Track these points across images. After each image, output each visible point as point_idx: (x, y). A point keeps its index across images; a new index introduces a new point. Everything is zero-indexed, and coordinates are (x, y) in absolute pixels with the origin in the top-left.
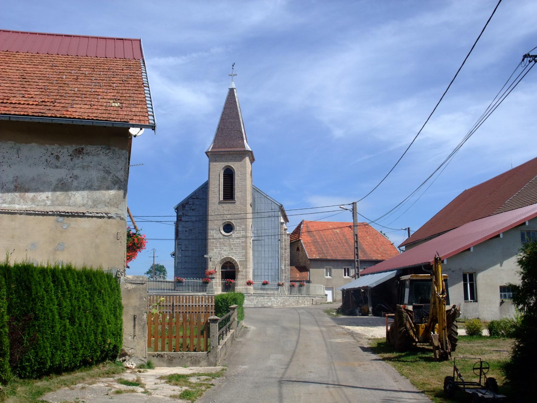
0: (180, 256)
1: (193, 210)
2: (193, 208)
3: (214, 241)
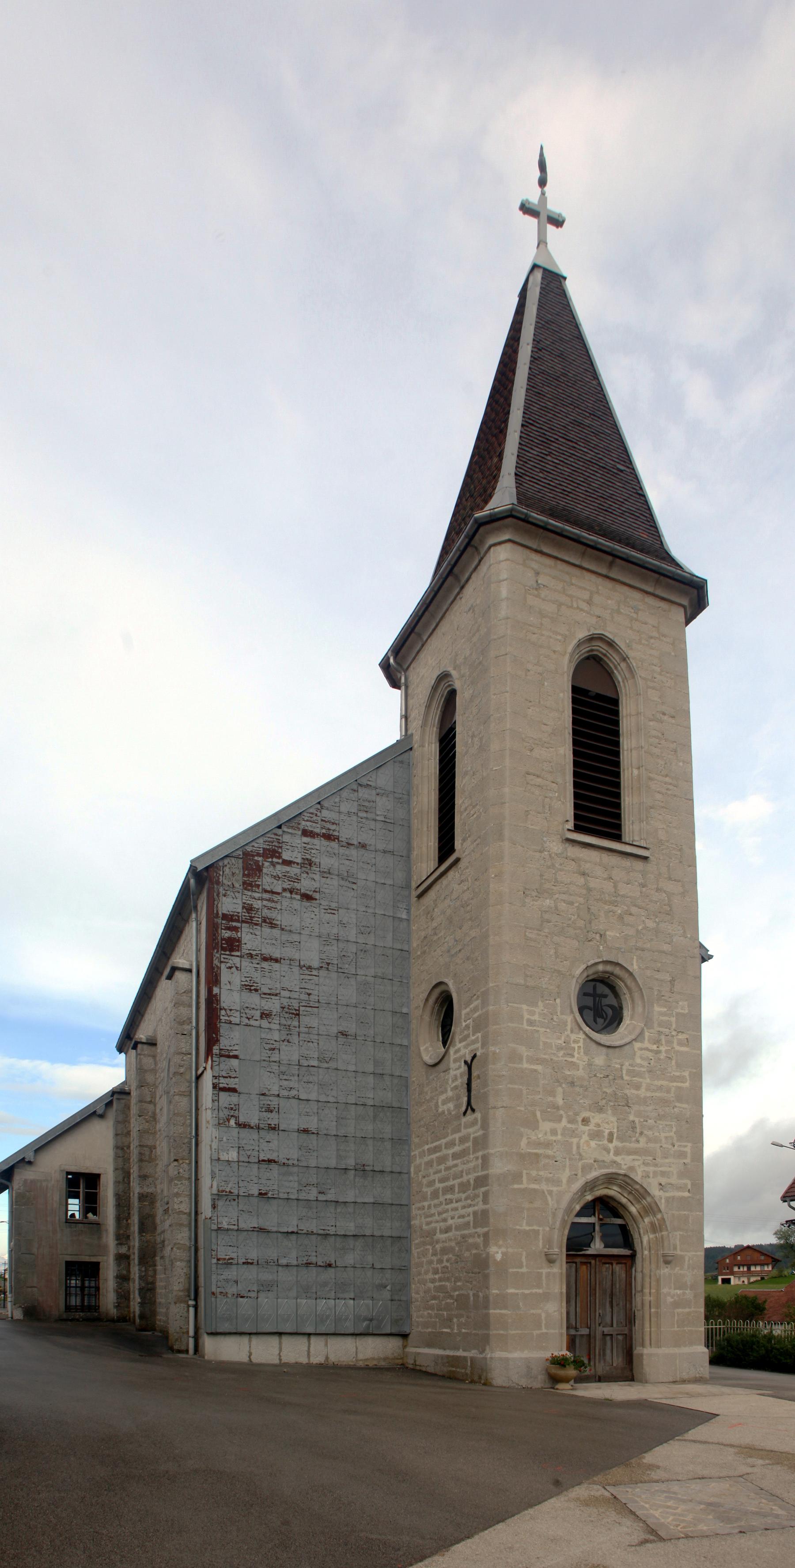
0: (233, 1155)
1: (307, 897)
2: (306, 884)
3: (539, 1068)
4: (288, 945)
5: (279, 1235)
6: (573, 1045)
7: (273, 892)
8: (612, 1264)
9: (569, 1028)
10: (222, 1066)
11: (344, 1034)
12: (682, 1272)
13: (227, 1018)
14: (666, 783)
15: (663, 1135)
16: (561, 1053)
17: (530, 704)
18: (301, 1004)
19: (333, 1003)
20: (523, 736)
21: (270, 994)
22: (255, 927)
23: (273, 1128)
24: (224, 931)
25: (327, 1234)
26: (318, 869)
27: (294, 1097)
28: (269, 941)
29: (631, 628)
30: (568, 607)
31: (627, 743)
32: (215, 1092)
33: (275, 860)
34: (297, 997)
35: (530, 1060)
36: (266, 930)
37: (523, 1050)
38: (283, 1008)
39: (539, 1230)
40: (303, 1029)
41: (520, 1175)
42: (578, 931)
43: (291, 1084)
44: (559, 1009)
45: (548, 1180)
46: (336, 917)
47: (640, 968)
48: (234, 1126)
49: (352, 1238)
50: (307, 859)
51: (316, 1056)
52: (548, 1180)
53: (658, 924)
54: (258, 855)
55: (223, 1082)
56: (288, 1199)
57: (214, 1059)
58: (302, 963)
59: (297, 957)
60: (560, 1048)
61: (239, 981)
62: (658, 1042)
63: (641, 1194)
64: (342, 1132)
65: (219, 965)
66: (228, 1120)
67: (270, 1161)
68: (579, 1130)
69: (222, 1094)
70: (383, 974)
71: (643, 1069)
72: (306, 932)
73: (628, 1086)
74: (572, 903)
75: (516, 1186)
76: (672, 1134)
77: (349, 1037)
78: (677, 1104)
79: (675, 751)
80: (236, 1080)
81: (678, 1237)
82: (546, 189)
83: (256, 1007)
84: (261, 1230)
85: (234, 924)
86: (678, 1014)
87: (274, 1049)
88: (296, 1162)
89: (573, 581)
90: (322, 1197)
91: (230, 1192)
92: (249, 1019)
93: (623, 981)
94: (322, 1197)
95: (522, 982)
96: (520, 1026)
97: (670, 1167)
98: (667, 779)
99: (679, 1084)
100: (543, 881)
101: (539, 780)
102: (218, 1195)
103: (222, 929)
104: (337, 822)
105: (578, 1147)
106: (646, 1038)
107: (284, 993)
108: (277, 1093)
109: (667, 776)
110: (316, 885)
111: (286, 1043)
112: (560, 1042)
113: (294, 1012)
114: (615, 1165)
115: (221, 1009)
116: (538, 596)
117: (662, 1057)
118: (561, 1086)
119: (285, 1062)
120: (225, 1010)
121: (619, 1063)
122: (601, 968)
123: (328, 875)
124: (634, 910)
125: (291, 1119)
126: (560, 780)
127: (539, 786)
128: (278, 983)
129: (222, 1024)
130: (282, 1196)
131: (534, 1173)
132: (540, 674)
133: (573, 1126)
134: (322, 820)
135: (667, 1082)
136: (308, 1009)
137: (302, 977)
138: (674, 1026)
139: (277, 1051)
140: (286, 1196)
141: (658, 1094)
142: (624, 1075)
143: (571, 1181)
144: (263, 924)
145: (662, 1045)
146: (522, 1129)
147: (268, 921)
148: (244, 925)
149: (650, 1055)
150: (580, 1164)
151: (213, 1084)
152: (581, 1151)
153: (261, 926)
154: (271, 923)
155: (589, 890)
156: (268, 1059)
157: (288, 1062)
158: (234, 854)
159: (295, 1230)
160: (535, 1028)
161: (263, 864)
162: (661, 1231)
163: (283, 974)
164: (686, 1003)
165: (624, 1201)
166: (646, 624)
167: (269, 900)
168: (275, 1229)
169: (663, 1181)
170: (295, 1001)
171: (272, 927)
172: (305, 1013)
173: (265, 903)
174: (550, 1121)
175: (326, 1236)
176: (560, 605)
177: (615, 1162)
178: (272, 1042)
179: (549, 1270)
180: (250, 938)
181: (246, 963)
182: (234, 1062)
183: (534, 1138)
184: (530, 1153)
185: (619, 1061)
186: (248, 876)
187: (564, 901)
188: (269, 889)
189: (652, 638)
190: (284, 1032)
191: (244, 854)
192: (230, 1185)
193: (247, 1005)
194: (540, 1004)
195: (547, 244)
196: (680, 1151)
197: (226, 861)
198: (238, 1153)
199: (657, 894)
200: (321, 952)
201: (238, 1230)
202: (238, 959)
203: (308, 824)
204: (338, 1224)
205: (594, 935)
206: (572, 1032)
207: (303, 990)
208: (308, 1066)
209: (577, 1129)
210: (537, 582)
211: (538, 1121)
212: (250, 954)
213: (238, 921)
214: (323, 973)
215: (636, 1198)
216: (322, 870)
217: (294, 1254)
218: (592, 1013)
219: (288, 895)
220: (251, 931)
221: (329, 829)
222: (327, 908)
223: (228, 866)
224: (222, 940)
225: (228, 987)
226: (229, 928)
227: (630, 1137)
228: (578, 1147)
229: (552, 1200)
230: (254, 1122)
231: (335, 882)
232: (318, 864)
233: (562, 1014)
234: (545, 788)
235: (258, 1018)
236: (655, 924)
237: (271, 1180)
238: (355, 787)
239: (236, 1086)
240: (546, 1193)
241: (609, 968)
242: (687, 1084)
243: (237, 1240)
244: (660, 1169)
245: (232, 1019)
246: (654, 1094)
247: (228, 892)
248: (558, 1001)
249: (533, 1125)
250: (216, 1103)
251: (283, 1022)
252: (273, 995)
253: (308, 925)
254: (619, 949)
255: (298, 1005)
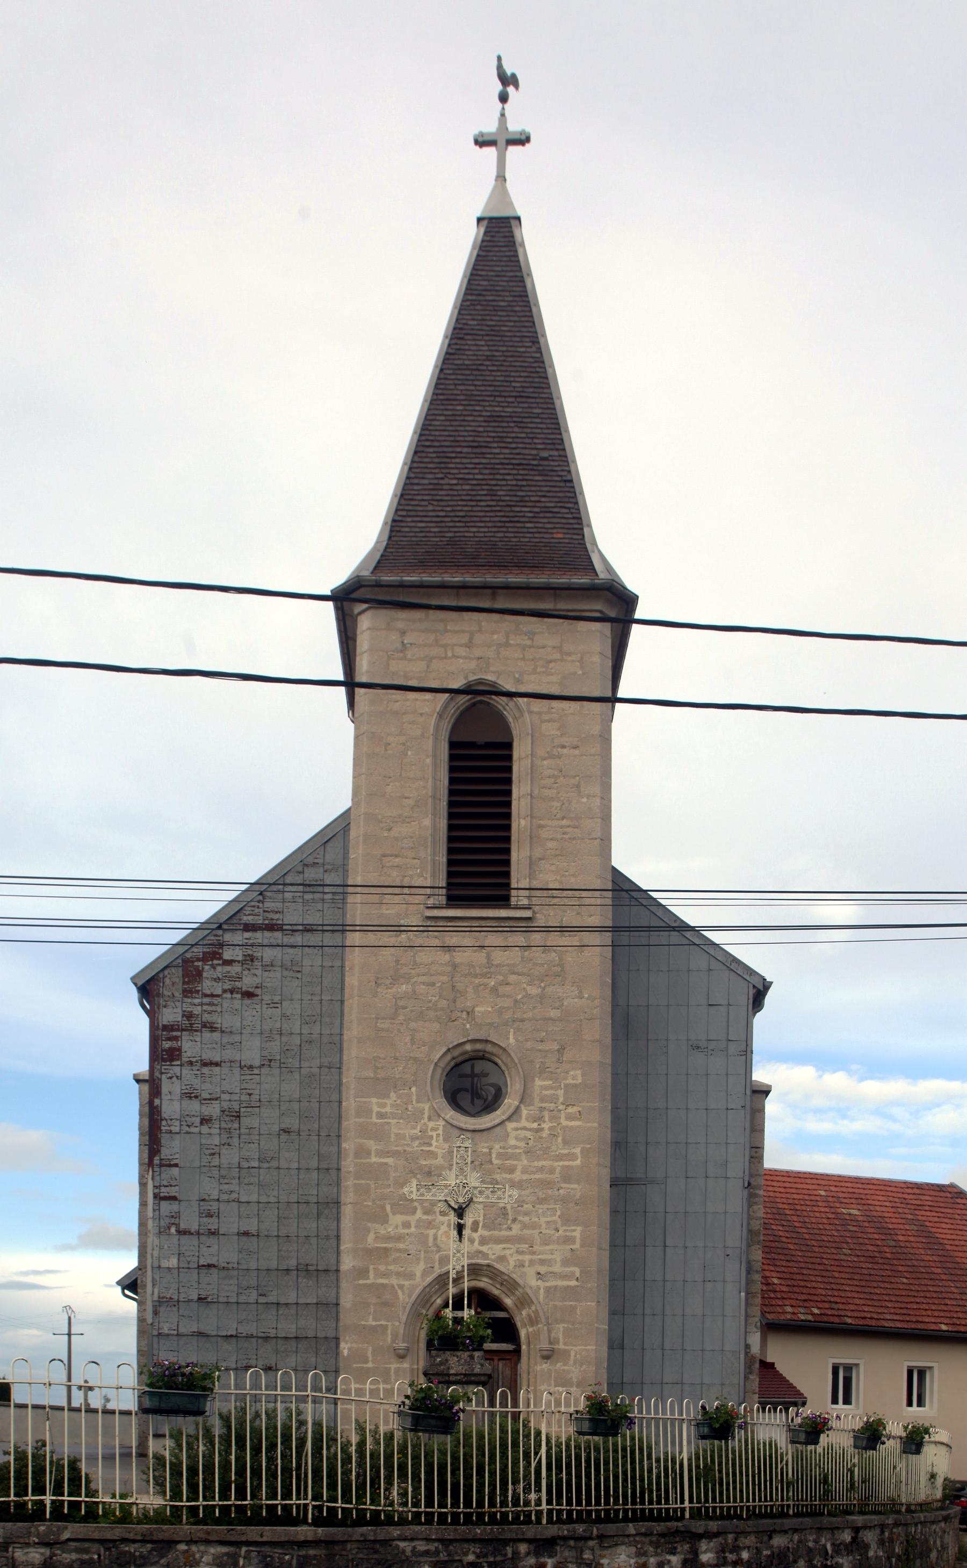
0: (173, 1262)
1: (249, 995)
2: (248, 982)
3: (390, 1161)
4: (229, 1047)
5: (219, 1339)
6: (430, 1133)
7: (212, 996)
8: (493, 1360)
9: (426, 1116)
10: (163, 1176)
11: (287, 1131)
12: (566, 1368)
13: (167, 1128)
14: (562, 827)
15: (543, 1220)
16: (417, 1143)
17: (390, 780)
18: (242, 1106)
19: (275, 1100)
20: (380, 817)
21: (210, 1099)
22: (195, 1033)
23: (213, 1233)
24: (164, 1042)
25: (269, 1337)
26: (260, 963)
27: (234, 1201)
28: (210, 1046)
29: (523, 659)
30: (441, 658)
31: (520, 791)
32: (157, 1202)
33: (215, 962)
34: (238, 1099)
35: (380, 1154)
36: (207, 1035)
37: (372, 1145)
38: (223, 1111)
39: (387, 1325)
40: (243, 1131)
41: (367, 1271)
42: (439, 1013)
43: (232, 1187)
44: (414, 1098)
45: (398, 1274)
46: (279, 1010)
47: (517, 1041)
48: (175, 1233)
49: (294, 1340)
50: (249, 955)
51: (257, 1157)
52: (398, 1274)
53: (544, 989)
54: (198, 960)
55: (164, 1192)
56: (227, 1302)
57: (155, 1169)
58: (243, 1064)
59: (238, 1058)
60: (414, 1138)
61: (179, 1090)
62: (540, 1119)
63: (511, 1285)
64: (283, 1232)
65: (159, 1076)
66: (169, 1228)
67: (209, 1266)
68: (437, 1221)
69: (163, 1204)
70: (330, 1063)
71: (518, 1151)
72: (248, 1030)
73: (499, 1171)
74: (433, 984)
75: (361, 1282)
76: (555, 1218)
77: (292, 1134)
78: (563, 1185)
79: (578, 786)
80: (177, 1188)
81: (562, 1329)
82: (506, 106)
83: (196, 1114)
84: (200, 1334)
85: (175, 1034)
86: (567, 1086)
87: (214, 1154)
88: (235, 1266)
89: (449, 628)
90: (262, 1300)
91: (171, 1298)
92: (189, 1126)
93: (499, 1058)
94: (262, 1300)
95: (372, 1075)
96: (369, 1120)
97: (552, 1254)
98: (564, 822)
99: (566, 1163)
100: (399, 967)
101: (397, 860)
102: (159, 1301)
103: (162, 1040)
104: (281, 910)
105: (435, 1238)
106: (524, 1116)
107: (224, 1097)
108: (217, 1197)
109: (563, 818)
110: (258, 980)
111: (226, 1147)
112: (415, 1131)
113: (235, 1114)
114: (480, 1255)
115: (162, 1120)
116: (404, 658)
117: (544, 1135)
118: (415, 1177)
119: (225, 1166)
120: (166, 1120)
121: (487, 1147)
122: (468, 1047)
123: (271, 968)
124: (512, 978)
125: (230, 1223)
126: (422, 855)
127: (397, 866)
128: (218, 1087)
129: (162, 1135)
130: (221, 1299)
131: (382, 1268)
132: (404, 744)
133: (430, 1218)
134: (265, 911)
135: (551, 1162)
136: (249, 1110)
137: (243, 1077)
138: (561, 1099)
139: (217, 1156)
140: (225, 1300)
141: (537, 1176)
142: (493, 1159)
143: (425, 1273)
144: (204, 1029)
145: (544, 1122)
146: (369, 1225)
147: (208, 1025)
148: (184, 1033)
149: (528, 1134)
150: (437, 1257)
151: (154, 1194)
152: (439, 1242)
153: (201, 1032)
154: (212, 1027)
155: (455, 966)
156: (208, 1164)
157: (228, 1166)
158: (174, 963)
159: (234, 1333)
160: (386, 1120)
161: (203, 968)
162: (537, 1324)
163: (223, 1077)
164: (579, 1072)
165: (496, 1292)
166: (543, 647)
167: (209, 1004)
168: (214, 1333)
169: (543, 1270)
170: (236, 1103)
171: (212, 1031)
172: (246, 1114)
173: (205, 1007)
174: (402, 1213)
175: (267, 1338)
176: (430, 660)
177: (480, 1252)
178: (212, 1147)
179: (398, 1366)
180: (190, 1046)
181: (186, 1071)
182: (175, 1171)
183: (383, 1232)
184: (377, 1248)
185: (487, 1145)
186: (188, 983)
187: (423, 983)
188: (208, 992)
189: (551, 661)
190: (225, 1136)
191: (184, 961)
192: (171, 1292)
193: (187, 1113)
194: (392, 1095)
195: (505, 180)
196: (566, 1236)
197: (166, 972)
198: (179, 1260)
199: (543, 955)
200: (262, 1049)
201: (178, 1335)
202: (179, 1068)
203: (250, 918)
204: (279, 1326)
205: (459, 1014)
206: (430, 1119)
207: (244, 1091)
208: (249, 1168)
209: (434, 1220)
210: (403, 642)
211: (387, 1215)
212: (190, 1061)
213: (177, 1030)
214: (265, 1070)
215: (509, 1290)
216: (264, 963)
217: (234, 1358)
218: (469, 1096)
219: (228, 995)
220: (191, 1038)
221: (272, 919)
222: (269, 1002)
223: (169, 976)
224: (163, 1051)
225: (169, 1097)
226: (169, 1039)
227: (500, 1224)
228: (435, 1238)
229: (403, 1294)
230: (194, 1228)
231: (277, 974)
232: (260, 958)
233: (418, 1102)
234: (404, 867)
235: (198, 1125)
236: (540, 989)
237: (211, 1284)
238: (300, 869)
239: (176, 1194)
240: (396, 1287)
241: (478, 1046)
242: (578, 1162)
243: (178, 1344)
244: (539, 1257)
245: (173, 1128)
246: (533, 1177)
247: (169, 1003)
248: (414, 1089)
249: (384, 1220)
250: (157, 1212)
251: (224, 1125)
252: (213, 1099)
253: (249, 1024)
254: (490, 1024)
255: (238, 1107)
